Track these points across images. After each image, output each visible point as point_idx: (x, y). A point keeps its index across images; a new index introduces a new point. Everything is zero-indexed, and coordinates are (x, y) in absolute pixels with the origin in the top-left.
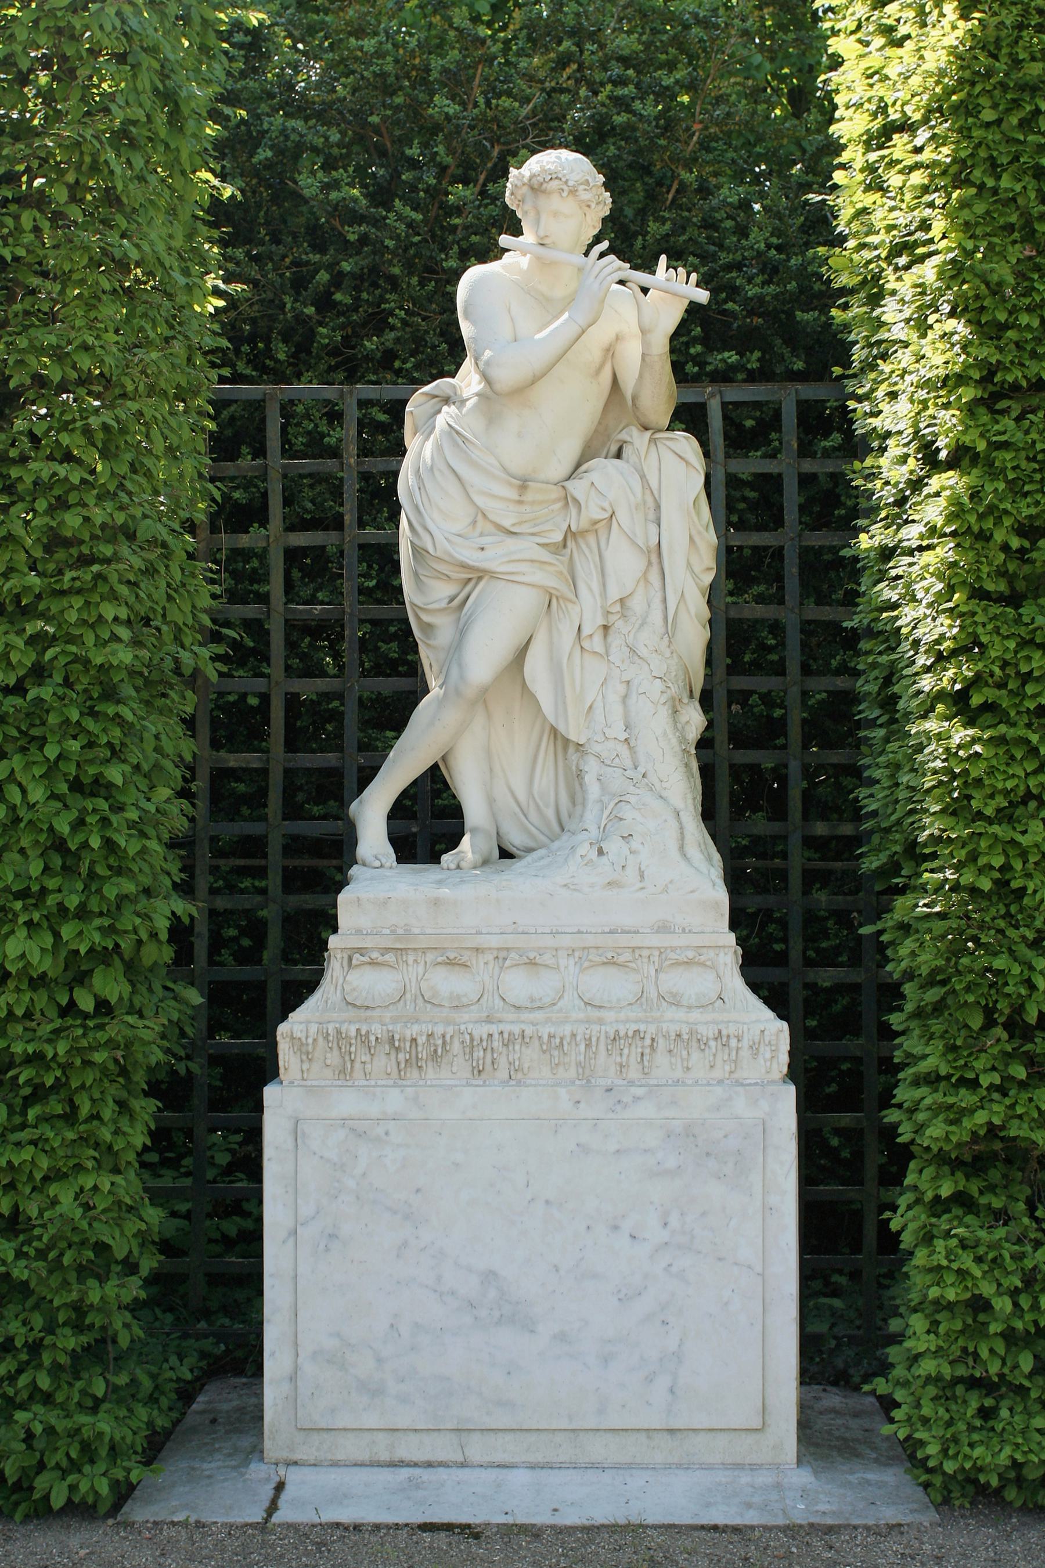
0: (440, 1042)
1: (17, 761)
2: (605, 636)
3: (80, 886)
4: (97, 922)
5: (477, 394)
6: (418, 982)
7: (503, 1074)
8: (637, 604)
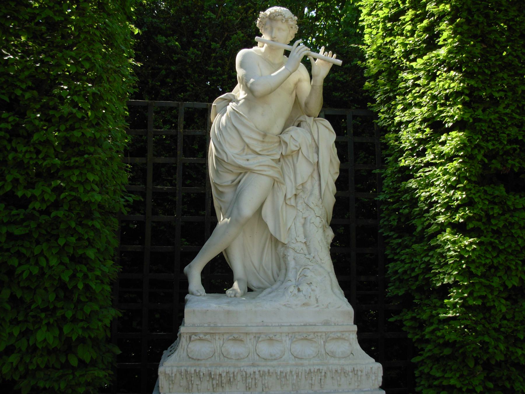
0: (232, 375)
1: (45, 246)
2: (296, 198)
3: (72, 306)
4: (81, 324)
5: (244, 98)
6: (221, 348)
7: (259, 389)
8: (308, 186)
